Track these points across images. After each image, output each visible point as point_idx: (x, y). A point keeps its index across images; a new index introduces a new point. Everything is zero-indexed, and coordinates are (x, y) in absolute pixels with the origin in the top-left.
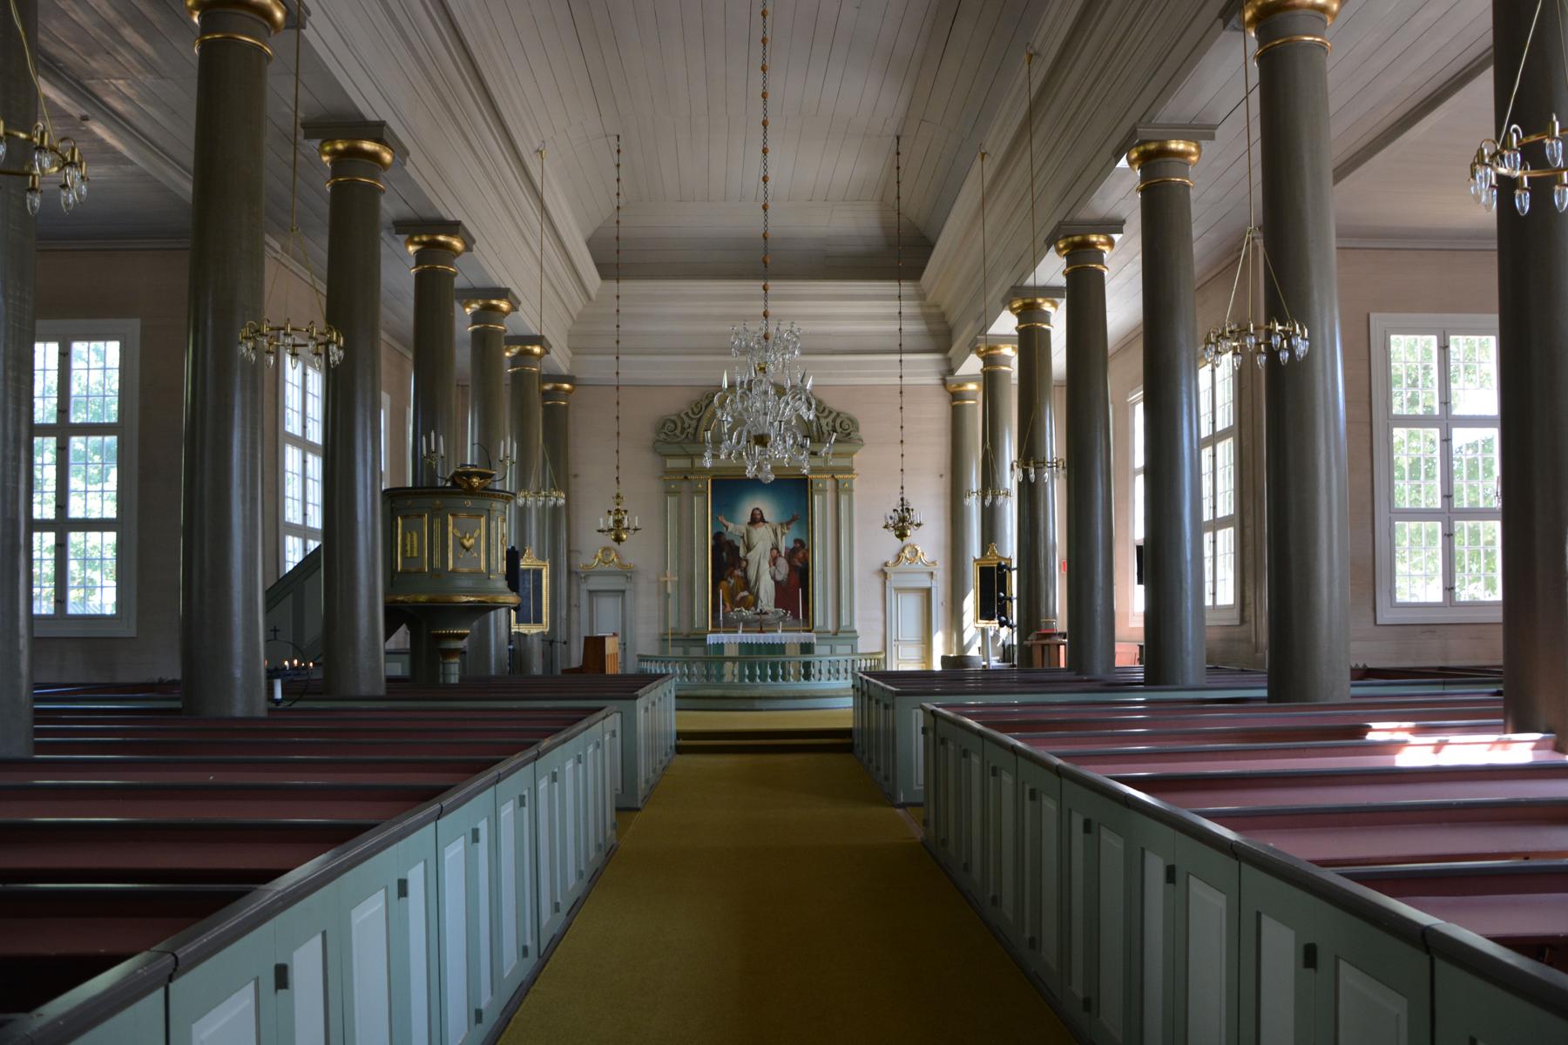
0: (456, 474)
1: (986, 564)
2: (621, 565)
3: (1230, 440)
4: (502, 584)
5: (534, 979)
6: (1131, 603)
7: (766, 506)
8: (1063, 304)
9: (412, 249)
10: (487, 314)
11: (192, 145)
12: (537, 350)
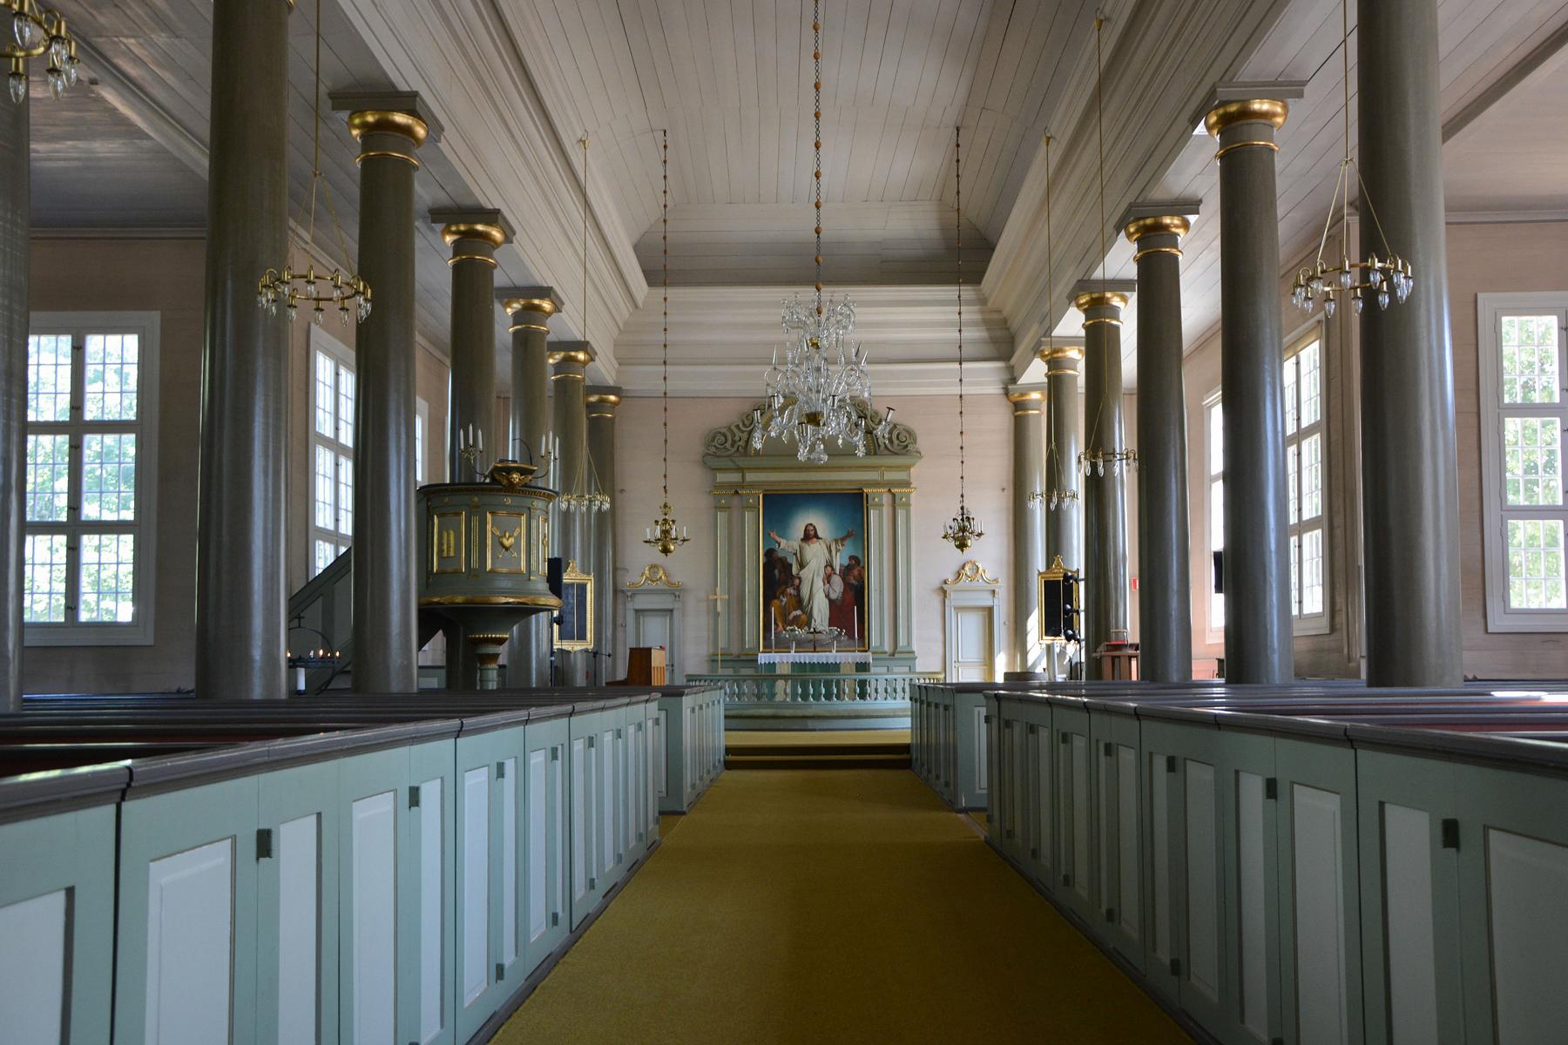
0: (496, 468)
1: (1051, 577)
2: (669, 583)
3: (1317, 437)
4: (543, 586)
5: (564, 951)
6: (1210, 615)
7: (819, 520)
8: (1133, 297)
9: (449, 239)
10: (529, 314)
11: (207, 114)
12: (581, 356)
